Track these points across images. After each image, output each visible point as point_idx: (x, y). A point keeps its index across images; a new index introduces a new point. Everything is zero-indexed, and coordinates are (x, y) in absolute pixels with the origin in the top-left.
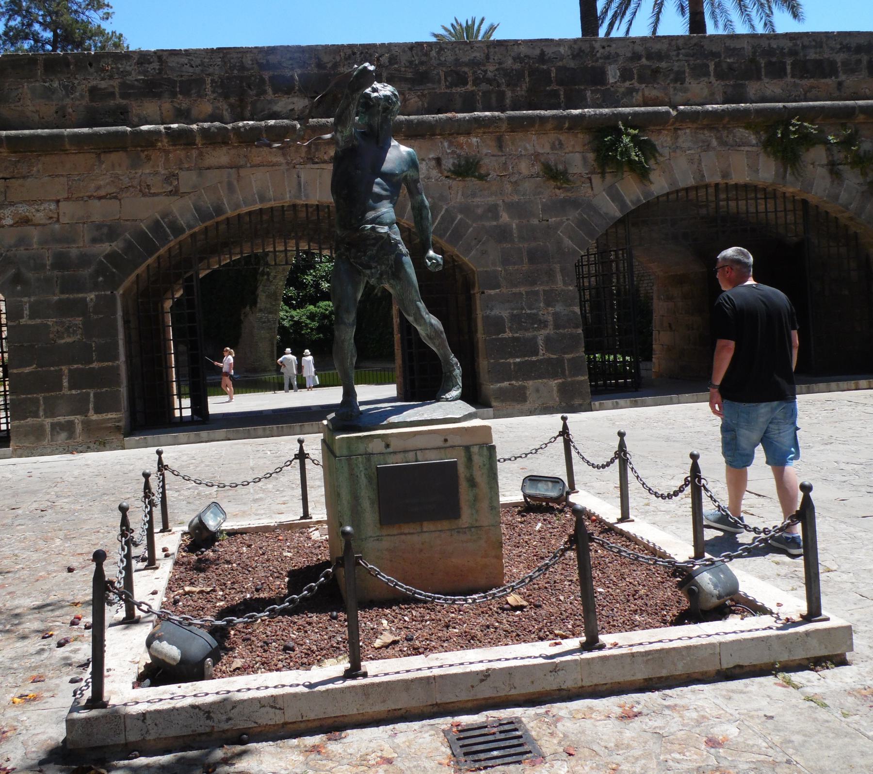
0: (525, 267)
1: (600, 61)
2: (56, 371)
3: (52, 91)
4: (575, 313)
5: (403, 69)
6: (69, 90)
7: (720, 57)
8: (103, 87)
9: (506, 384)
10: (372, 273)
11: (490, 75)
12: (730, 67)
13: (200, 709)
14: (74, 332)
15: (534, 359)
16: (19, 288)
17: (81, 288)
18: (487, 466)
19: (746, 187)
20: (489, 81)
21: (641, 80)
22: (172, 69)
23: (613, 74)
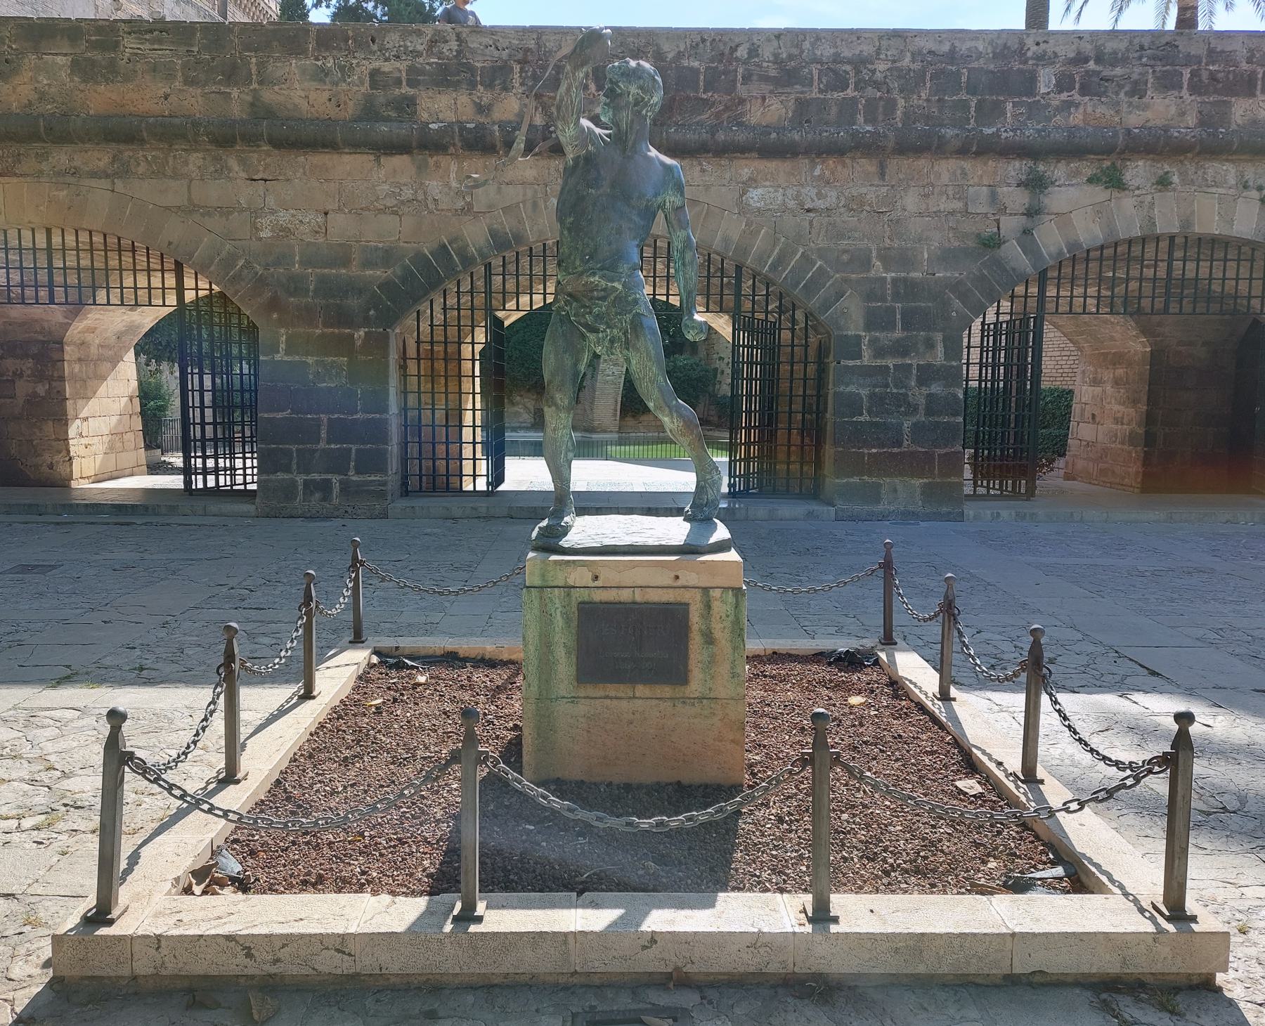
0: (898, 334)
1: (1030, 62)
2: (313, 419)
4: (955, 396)
5: (765, 64)
6: (346, 71)
7: (1200, 62)
9: (856, 479)
10: (599, 339)
11: (878, 76)
12: (1213, 77)
13: (237, 942)
15: (896, 450)
16: (275, 316)
18: (732, 618)
19: (1214, 241)
20: (877, 85)
21: (1084, 91)
22: (473, 51)
23: (1046, 80)
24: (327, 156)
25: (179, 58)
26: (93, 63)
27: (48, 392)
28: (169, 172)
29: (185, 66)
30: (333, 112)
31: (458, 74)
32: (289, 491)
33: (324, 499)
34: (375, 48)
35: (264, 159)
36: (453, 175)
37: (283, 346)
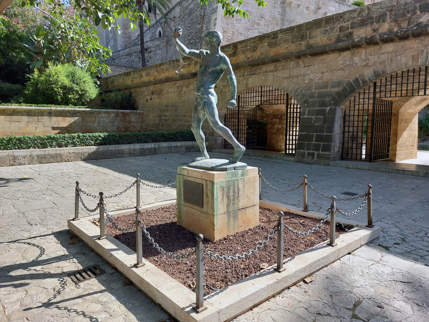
3: (327, 31)
8: (344, 25)
14: (320, 121)
17: (326, 106)
22: (373, 12)
24: (325, 56)
25: (291, 36)
26: (272, 43)
27: (281, 127)
28: (286, 68)
29: (292, 38)
30: (328, 42)
31: (367, 21)
32: (303, 155)
33: (312, 158)
34: (341, 19)
35: (308, 60)
36: (363, 54)
37: (307, 113)
